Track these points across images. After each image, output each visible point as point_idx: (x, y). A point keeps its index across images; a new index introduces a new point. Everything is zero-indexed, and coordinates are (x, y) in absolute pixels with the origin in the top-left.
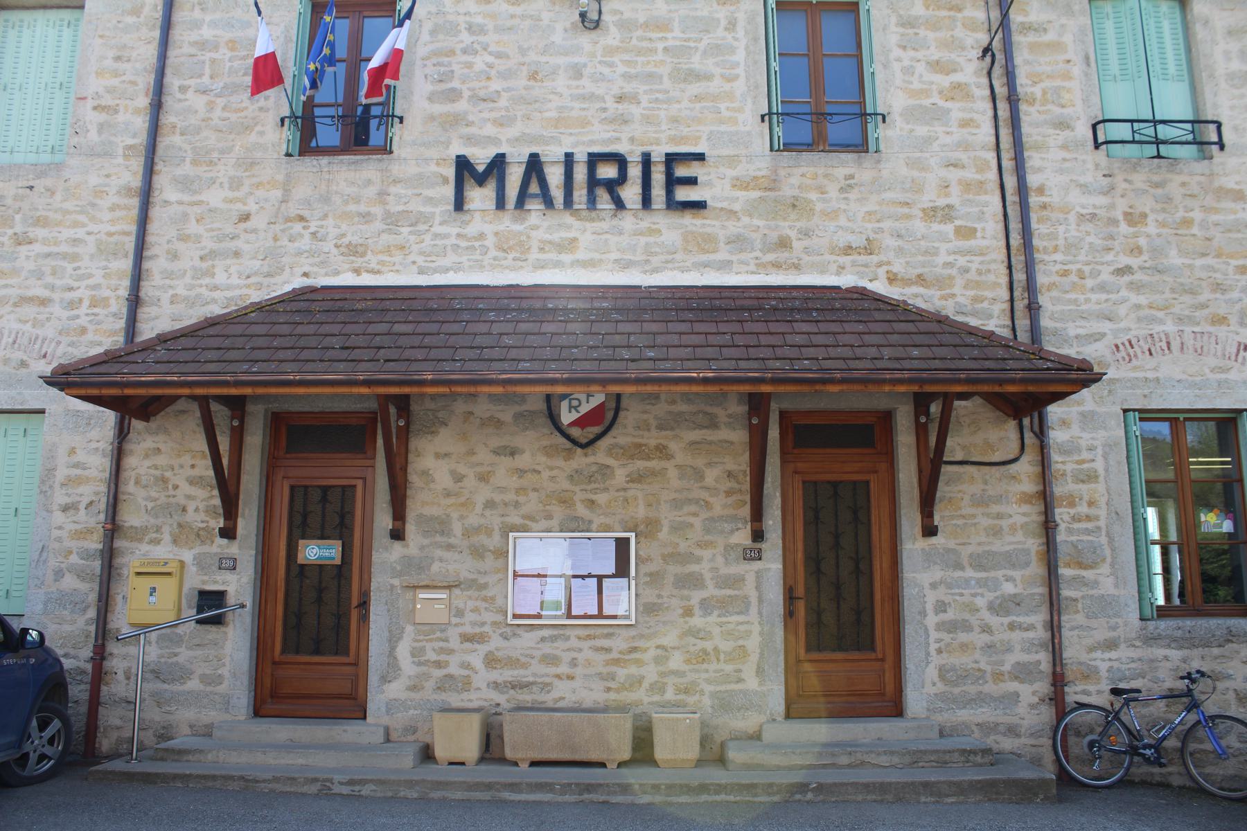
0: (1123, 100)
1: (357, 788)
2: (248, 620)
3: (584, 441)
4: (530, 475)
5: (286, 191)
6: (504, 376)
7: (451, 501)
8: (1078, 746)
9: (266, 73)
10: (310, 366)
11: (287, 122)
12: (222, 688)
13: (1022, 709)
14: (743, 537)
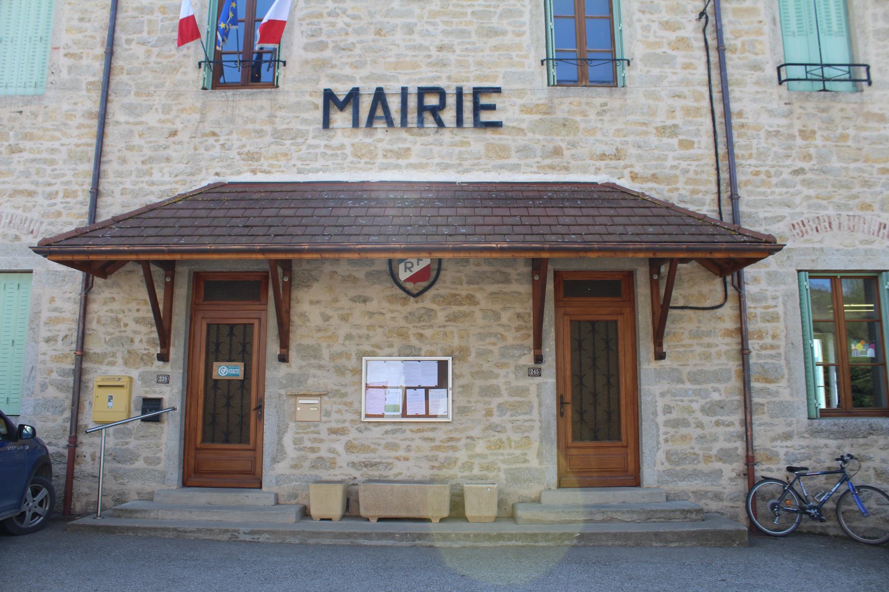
0: (800, 50)
1: (256, 537)
2: (178, 418)
3: (416, 292)
7: (321, 334)
8: (764, 507)
9: (188, 30)
10: (221, 240)
11: (203, 65)
12: (160, 467)
13: (724, 481)
14: (528, 360)
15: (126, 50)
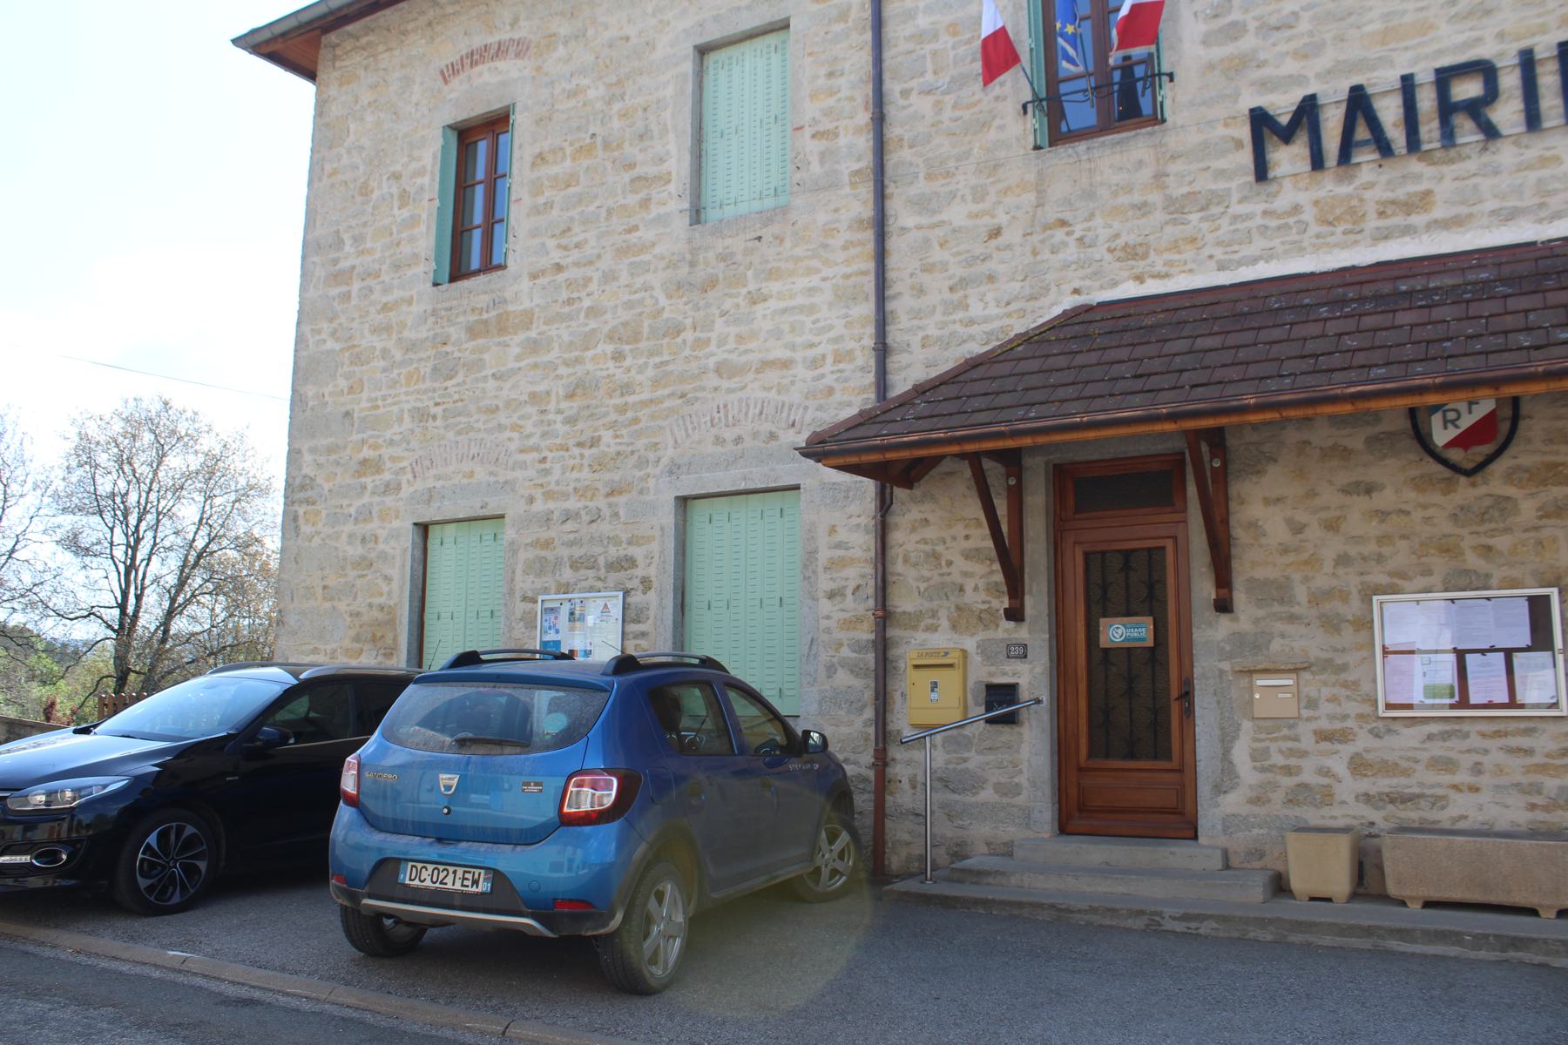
1: (1193, 925)
2: (1046, 717)
3: (1469, 466)
4: (1394, 517)
5: (1039, 192)
6: (1353, 390)
7: (1291, 558)
9: (997, 55)
10: (1098, 403)
11: (1030, 108)
12: (1020, 800)
15: (904, 108)
